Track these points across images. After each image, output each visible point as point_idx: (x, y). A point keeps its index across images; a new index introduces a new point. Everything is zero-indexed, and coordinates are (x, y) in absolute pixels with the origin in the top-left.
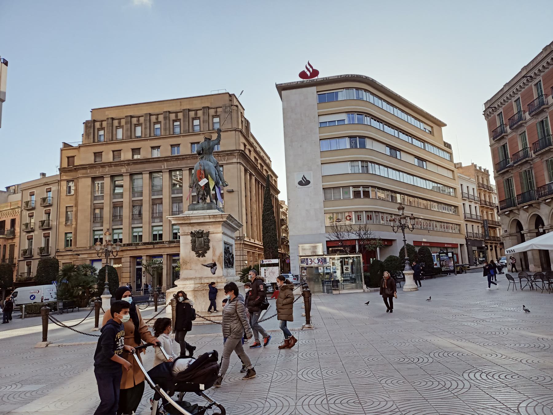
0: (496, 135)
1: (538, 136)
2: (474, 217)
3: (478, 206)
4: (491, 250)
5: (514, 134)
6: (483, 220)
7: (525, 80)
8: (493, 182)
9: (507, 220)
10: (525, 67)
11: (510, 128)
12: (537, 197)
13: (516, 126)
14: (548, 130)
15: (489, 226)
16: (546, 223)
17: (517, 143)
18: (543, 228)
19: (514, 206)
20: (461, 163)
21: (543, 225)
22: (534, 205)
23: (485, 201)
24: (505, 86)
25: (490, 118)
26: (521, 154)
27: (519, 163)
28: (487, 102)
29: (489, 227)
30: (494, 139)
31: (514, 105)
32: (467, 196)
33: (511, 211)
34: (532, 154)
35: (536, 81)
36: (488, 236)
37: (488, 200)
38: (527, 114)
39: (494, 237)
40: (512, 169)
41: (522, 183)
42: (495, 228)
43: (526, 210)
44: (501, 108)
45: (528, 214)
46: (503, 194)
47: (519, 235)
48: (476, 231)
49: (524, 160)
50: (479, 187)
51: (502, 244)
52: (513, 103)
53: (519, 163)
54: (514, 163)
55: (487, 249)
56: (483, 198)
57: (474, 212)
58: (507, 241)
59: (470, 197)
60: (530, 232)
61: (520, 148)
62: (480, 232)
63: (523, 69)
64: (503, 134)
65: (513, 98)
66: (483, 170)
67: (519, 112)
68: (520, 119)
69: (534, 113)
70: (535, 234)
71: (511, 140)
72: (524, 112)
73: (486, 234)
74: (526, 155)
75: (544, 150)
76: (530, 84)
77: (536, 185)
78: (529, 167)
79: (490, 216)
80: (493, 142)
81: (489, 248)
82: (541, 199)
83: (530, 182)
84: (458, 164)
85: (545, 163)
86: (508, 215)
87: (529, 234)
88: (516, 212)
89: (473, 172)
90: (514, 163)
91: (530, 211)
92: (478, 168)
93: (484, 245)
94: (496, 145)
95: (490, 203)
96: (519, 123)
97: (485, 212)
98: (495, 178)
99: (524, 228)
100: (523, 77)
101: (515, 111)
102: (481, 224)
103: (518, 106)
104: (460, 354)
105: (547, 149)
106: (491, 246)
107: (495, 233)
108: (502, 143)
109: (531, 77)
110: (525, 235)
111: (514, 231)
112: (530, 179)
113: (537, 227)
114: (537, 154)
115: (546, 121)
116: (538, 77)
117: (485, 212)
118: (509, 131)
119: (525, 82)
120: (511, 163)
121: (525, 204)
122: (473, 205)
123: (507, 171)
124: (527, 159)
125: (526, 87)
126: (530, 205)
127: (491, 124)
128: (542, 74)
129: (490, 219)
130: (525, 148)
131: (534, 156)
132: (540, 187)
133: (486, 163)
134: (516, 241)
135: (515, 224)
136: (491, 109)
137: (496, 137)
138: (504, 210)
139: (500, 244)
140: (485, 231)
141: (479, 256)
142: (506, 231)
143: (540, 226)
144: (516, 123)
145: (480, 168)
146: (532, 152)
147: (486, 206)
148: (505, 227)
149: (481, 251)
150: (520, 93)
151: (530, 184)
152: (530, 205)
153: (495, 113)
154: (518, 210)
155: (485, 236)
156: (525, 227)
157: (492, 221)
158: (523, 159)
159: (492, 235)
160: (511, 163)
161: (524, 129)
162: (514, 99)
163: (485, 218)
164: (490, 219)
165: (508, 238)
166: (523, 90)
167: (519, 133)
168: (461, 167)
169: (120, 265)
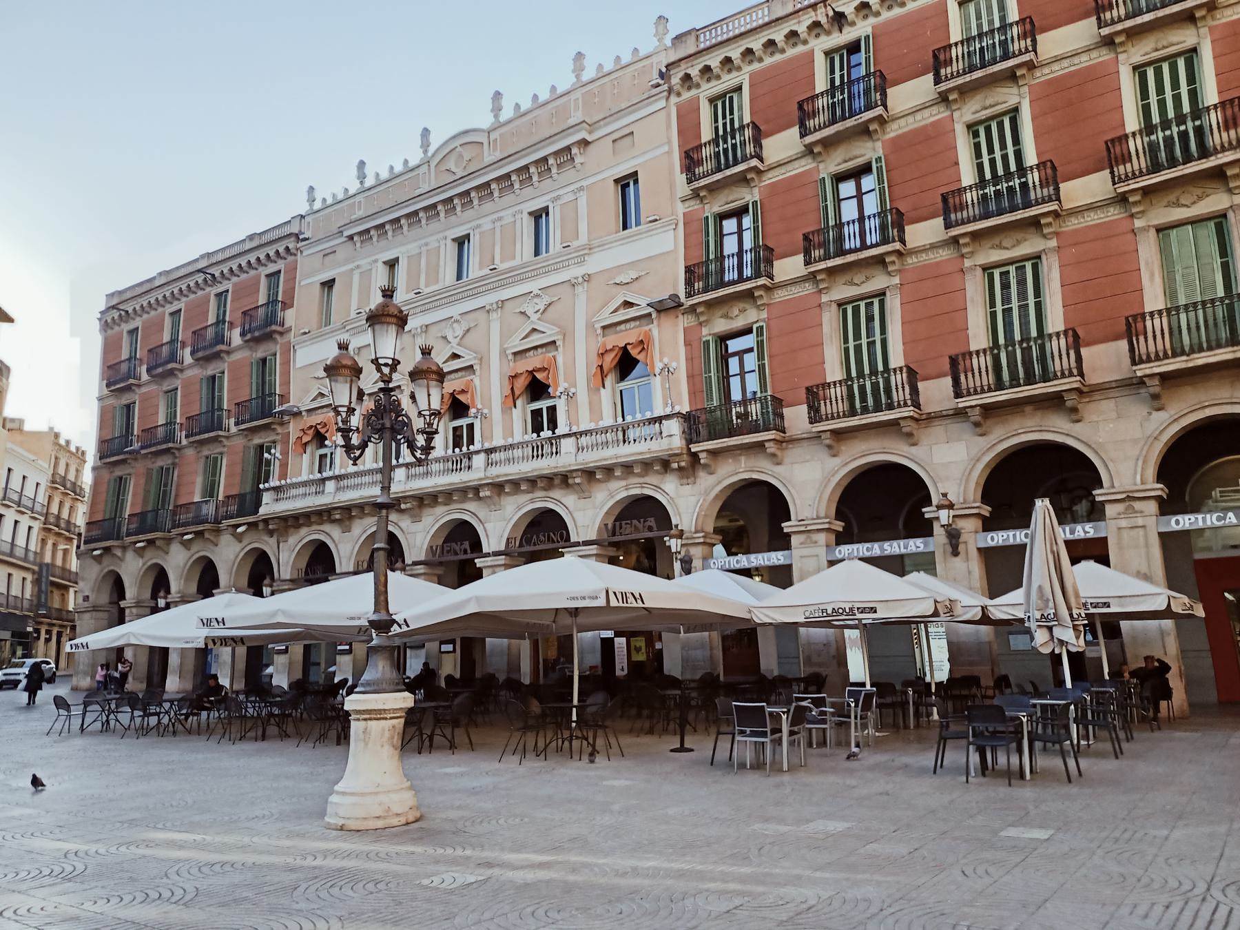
0: (117, 378)
1: (247, 391)
2: (19, 552)
3: (37, 526)
4: (48, 640)
5: (154, 387)
6: (41, 565)
7: (200, 278)
8: (87, 479)
9: (94, 572)
10: (209, 255)
11: (148, 371)
12: (169, 525)
13: (160, 370)
14: (221, 399)
15: (51, 581)
16: (174, 587)
17: (155, 408)
18: (165, 598)
19: (118, 538)
20: (21, 421)
21: (168, 591)
22: (158, 543)
23: (58, 517)
24: (160, 274)
25: (109, 332)
26: (161, 432)
27: (153, 449)
28: (112, 295)
29: (53, 584)
30: (108, 385)
31: (168, 322)
32: (15, 497)
33: (107, 550)
34: (181, 436)
35: (221, 288)
36: (45, 606)
37: (65, 515)
38: (188, 350)
39: (60, 610)
40: (136, 459)
41: (147, 492)
42: (66, 588)
43: (140, 552)
44: (138, 319)
45: (141, 562)
46: (101, 507)
47: (115, 610)
48: (15, 591)
49: (164, 446)
50: (53, 482)
51: (73, 628)
52: (167, 317)
53: (153, 449)
54: (142, 448)
55: (38, 638)
56: (54, 509)
57: (21, 541)
58: (83, 622)
59: (25, 501)
60: (138, 604)
61: (161, 420)
62: (28, 595)
63: (202, 257)
64: (132, 381)
65: (168, 306)
66: (73, 449)
67: (173, 341)
68: (173, 357)
69: (200, 354)
70: (148, 611)
71: (145, 399)
72: (184, 345)
73: (39, 601)
74: (170, 437)
75: (206, 436)
76: (208, 289)
77: (175, 500)
78: (170, 462)
79: (60, 555)
80: (106, 391)
81: (43, 636)
82: (175, 532)
83: (165, 492)
84: (13, 420)
85: (203, 460)
86: (98, 559)
87: (134, 610)
88: (118, 553)
89: (48, 447)
90: (142, 448)
91: (149, 553)
92: (62, 442)
93: (30, 629)
94: (111, 401)
95: (68, 522)
96: (170, 366)
97: (50, 543)
98: (94, 469)
99: (128, 595)
100: (199, 271)
101: (166, 337)
102: (34, 572)
103: (175, 326)
104: (127, 898)
105: (212, 434)
106: (48, 632)
107: (64, 599)
108: (125, 399)
109: (213, 275)
110: (127, 611)
111: (104, 598)
112: (166, 485)
113: (154, 596)
114: (192, 439)
115: (221, 379)
116: (226, 282)
117: (50, 543)
118: (145, 377)
119: (200, 281)
120: (136, 446)
121: (141, 537)
122: (25, 522)
123: (123, 461)
124: (171, 445)
125: (200, 293)
126: (151, 542)
127: (110, 347)
128: (235, 279)
129: (59, 562)
130: (170, 423)
131: (184, 442)
132: (181, 506)
133: (81, 427)
134: (105, 623)
135: (111, 581)
136: (118, 312)
137: (115, 383)
138: (93, 546)
139: (67, 625)
140: (40, 591)
141: (14, 653)
142: (86, 598)
143: (162, 594)
144: (163, 365)
145: (68, 442)
146: (184, 433)
147: (55, 527)
148: (85, 587)
149: (20, 644)
150: (184, 299)
151: (163, 497)
152: (151, 542)
153: (123, 325)
154: (124, 548)
155: (39, 605)
156: (130, 593)
157: (63, 569)
158: (161, 444)
159: (56, 605)
160: (136, 446)
161: (177, 383)
162: (171, 308)
163: (48, 559)
164: (59, 562)
165: (87, 616)
166: (192, 296)
167: (165, 388)
168: (20, 430)
169: (764, 315)
